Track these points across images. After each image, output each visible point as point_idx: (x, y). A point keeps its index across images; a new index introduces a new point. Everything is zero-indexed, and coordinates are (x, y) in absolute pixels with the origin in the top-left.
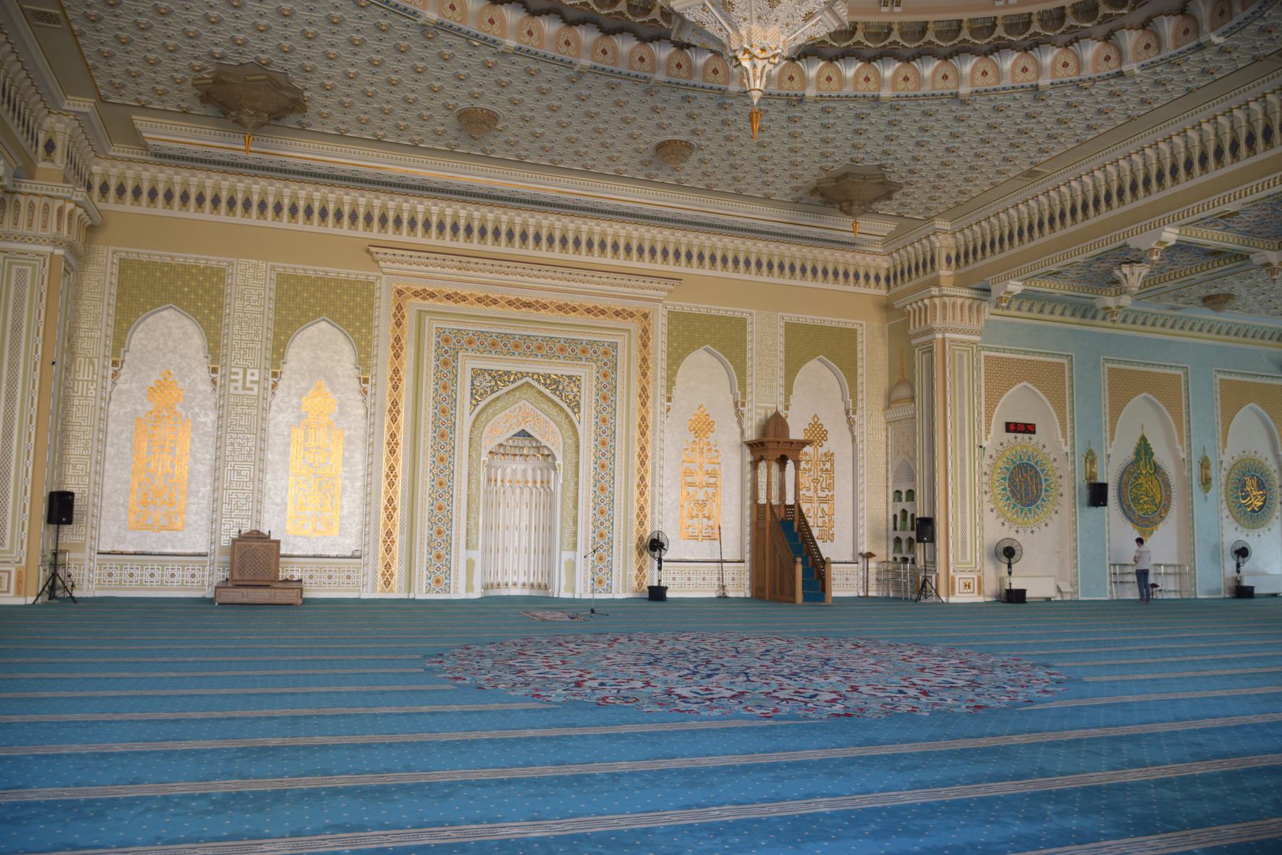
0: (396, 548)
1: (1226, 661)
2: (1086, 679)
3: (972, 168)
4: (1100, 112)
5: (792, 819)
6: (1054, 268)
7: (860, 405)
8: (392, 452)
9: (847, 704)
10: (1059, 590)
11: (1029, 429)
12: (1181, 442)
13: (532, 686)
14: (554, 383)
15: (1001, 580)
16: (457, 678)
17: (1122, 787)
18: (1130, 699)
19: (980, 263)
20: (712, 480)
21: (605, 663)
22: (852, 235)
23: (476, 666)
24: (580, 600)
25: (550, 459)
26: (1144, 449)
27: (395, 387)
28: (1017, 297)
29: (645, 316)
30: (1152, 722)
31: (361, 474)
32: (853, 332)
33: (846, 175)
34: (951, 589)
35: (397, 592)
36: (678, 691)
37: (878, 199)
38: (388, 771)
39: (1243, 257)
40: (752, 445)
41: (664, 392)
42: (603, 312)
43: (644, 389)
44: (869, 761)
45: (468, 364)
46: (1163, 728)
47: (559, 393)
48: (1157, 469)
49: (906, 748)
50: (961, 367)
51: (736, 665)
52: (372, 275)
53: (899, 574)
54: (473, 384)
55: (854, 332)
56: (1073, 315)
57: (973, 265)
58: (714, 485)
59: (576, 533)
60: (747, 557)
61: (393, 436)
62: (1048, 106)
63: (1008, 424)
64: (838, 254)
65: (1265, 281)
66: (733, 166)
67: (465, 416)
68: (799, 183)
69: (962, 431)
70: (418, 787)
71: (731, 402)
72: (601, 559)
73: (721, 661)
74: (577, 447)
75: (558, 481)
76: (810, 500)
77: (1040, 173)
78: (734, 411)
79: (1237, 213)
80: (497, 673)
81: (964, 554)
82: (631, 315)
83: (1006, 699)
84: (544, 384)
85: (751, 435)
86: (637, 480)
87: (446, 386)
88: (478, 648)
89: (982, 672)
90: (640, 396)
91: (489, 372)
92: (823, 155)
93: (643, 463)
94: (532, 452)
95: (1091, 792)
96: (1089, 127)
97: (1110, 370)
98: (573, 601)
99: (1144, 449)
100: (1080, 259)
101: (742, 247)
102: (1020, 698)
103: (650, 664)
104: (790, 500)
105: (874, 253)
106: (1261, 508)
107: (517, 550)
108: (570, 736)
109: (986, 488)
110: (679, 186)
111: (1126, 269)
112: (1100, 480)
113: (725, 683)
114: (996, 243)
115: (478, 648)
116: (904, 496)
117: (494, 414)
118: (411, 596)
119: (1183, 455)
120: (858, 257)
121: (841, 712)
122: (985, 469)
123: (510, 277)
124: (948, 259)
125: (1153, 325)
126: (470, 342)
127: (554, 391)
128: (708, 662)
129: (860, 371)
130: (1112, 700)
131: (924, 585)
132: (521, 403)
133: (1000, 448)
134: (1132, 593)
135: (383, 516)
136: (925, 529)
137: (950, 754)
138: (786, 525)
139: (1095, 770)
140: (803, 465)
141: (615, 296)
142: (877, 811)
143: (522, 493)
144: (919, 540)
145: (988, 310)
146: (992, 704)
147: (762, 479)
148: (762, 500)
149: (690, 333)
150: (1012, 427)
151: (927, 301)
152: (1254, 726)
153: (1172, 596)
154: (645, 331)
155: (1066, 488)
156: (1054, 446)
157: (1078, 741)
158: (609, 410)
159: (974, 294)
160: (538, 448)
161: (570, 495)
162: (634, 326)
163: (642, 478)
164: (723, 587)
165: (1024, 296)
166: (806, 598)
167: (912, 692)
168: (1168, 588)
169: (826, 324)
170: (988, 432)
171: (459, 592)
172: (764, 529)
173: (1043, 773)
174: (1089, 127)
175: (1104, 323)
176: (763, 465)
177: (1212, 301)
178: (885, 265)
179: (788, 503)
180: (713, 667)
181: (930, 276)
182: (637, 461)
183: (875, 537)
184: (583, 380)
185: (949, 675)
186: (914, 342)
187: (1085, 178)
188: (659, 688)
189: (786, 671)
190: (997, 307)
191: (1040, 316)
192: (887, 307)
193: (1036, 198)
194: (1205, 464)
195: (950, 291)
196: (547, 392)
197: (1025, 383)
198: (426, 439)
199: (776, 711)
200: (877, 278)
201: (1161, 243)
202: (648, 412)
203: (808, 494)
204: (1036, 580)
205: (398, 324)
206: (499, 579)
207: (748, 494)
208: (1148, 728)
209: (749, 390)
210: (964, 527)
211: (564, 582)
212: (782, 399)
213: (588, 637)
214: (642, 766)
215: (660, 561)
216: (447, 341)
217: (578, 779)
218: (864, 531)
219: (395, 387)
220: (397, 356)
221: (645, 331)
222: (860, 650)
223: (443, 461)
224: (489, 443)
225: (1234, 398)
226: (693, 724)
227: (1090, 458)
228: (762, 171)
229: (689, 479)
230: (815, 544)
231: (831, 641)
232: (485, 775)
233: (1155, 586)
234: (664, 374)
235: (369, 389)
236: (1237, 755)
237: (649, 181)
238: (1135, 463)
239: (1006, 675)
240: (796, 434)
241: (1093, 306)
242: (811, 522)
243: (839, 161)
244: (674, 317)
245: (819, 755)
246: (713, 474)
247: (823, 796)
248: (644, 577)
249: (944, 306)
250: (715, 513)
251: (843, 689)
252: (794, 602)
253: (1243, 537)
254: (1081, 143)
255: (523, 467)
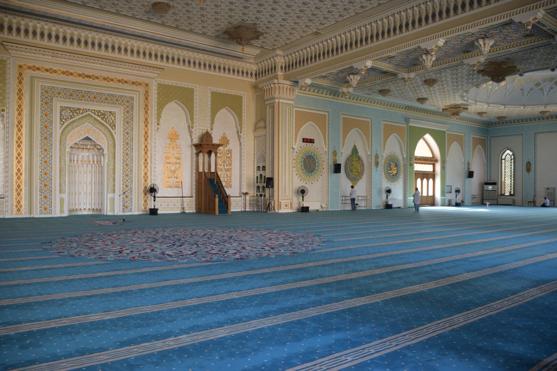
0: (23, 193)
1: (384, 232)
2: (334, 240)
3: (293, 28)
4: (345, 9)
5: (223, 301)
6: (324, 74)
7: (243, 129)
8: (19, 146)
9: (241, 254)
10: (322, 207)
11: (311, 141)
12: (369, 148)
13: (98, 254)
14: (103, 115)
15: (299, 203)
16: (60, 252)
17: (351, 280)
18: (351, 247)
19: (294, 70)
20: (178, 161)
21: (132, 242)
22: (242, 54)
23: (69, 246)
24: (117, 216)
25: (101, 151)
26: (355, 150)
27: (20, 114)
28: (309, 86)
29: (147, 85)
30: (360, 255)
31: (2, 157)
32: (241, 97)
33: (240, 26)
34: (280, 207)
35: (24, 214)
36: (167, 253)
37: (253, 39)
38: (30, 296)
39: (395, 75)
40: (196, 146)
41: (156, 121)
42: (126, 82)
43: (146, 119)
44: (252, 277)
45: (58, 104)
46: (363, 257)
47: (105, 120)
48: (359, 158)
49: (266, 270)
50: (286, 114)
51: (192, 241)
52: (5, 57)
53: (258, 201)
54: (61, 114)
55: (241, 97)
56: (330, 95)
57: (292, 71)
58: (179, 163)
59: (114, 185)
60: (194, 195)
61: (19, 138)
62: (325, 4)
63: (303, 139)
64: (235, 62)
65: (402, 85)
66: (189, 18)
67: (57, 129)
68: (218, 28)
69: (285, 141)
70: (47, 302)
71: (187, 126)
72: (127, 197)
73: (185, 239)
74: (115, 145)
75: (105, 161)
76: (221, 170)
77: (319, 33)
78: (188, 130)
79: (394, 57)
80: (80, 249)
81: (285, 193)
82: (140, 84)
83: (304, 249)
84: (98, 115)
85: (196, 141)
86: (143, 161)
87: (47, 115)
88: (69, 238)
89: (294, 239)
90: (145, 122)
91: (70, 108)
92: (230, 16)
93: (146, 153)
94: (92, 147)
95: (339, 282)
96: (340, 16)
97: (344, 118)
98: (114, 216)
99: (355, 150)
100: (334, 71)
101: (192, 56)
102: (310, 249)
103: (153, 242)
104: (213, 170)
105: (250, 63)
106: (396, 174)
107: (86, 193)
108: (119, 275)
109: (294, 165)
110: (163, 24)
111: (351, 77)
112: (338, 162)
113: (188, 248)
114: (301, 62)
115: (69, 238)
116: (261, 169)
117: (72, 129)
118: (32, 216)
119: (369, 153)
120: (244, 64)
121: (239, 257)
122: (294, 157)
123: (79, 62)
124: (282, 68)
125: (360, 100)
126: (59, 93)
127: (102, 119)
128: (179, 240)
129: (243, 114)
130: (344, 248)
131: (269, 206)
132: (86, 124)
133: (300, 149)
134: (349, 207)
135: (15, 178)
136: (270, 182)
137: (284, 272)
138: (211, 181)
139: (340, 274)
140: (218, 155)
141: (132, 75)
142: (257, 296)
143: (87, 166)
144: (267, 187)
145: (297, 90)
146: (299, 251)
147: (201, 161)
148: (201, 170)
149: (167, 94)
150: (305, 140)
151: (272, 85)
152: (396, 255)
153: (363, 208)
154: (147, 92)
155: (325, 166)
156: (321, 149)
157: (333, 264)
158: (130, 128)
159: (291, 83)
160: (95, 145)
161: (111, 167)
162: (142, 89)
163: (146, 160)
164: (183, 208)
165: (312, 85)
166: (219, 213)
167: (267, 248)
168: (362, 205)
169: (229, 93)
170: (296, 142)
171: (57, 214)
172: (202, 183)
173: (321, 277)
174: (340, 16)
175: (342, 99)
176: (201, 155)
177: (383, 92)
178: (255, 68)
179: (212, 171)
180: (182, 242)
181: (274, 74)
182: (143, 152)
183: (249, 186)
184: (117, 114)
185: (281, 241)
186: (266, 103)
187: (357, 30)
188: (159, 252)
189: (214, 242)
190: (301, 89)
191: (317, 94)
192: (255, 87)
193: (331, 39)
194: (377, 157)
195: (282, 82)
196: (99, 119)
197: (311, 122)
198: (37, 140)
199: (211, 258)
200: (251, 74)
201: (366, 67)
202: (148, 130)
203: (221, 167)
204: (313, 203)
205: (20, 83)
206: (77, 207)
207: (194, 167)
208: (358, 258)
209: (195, 121)
210: (285, 181)
211: (109, 208)
212: (209, 125)
213: (123, 232)
214: (154, 285)
215: (155, 197)
216: (47, 92)
217: (125, 293)
218: (244, 184)
219: (20, 114)
220: (20, 98)
221: (147, 92)
222: (244, 233)
223: (46, 150)
224: (70, 142)
225: (389, 130)
226: (176, 266)
227: (335, 153)
228: (202, 21)
229: (168, 161)
230: (224, 189)
231: (232, 229)
232: (79, 294)
233: (357, 204)
234: (156, 113)
235: (5, 115)
236: (390, 266)
237: (148, 21)
238: (351, 156)
239: (304, 240)
240: (216, 141)
241: (338, 91)
242: (222, 179)
243: (237, 20)
244: (160, 86)
245: (231, 275)
246: (179, 158)
247: (234, 291)
248: (147, 204)
249: (279, 88)
250: (179, 176)
251: (239, 248)
252: (215, 214)
253: (389, 186)
254: (337, 22)
255: (88, 154)
